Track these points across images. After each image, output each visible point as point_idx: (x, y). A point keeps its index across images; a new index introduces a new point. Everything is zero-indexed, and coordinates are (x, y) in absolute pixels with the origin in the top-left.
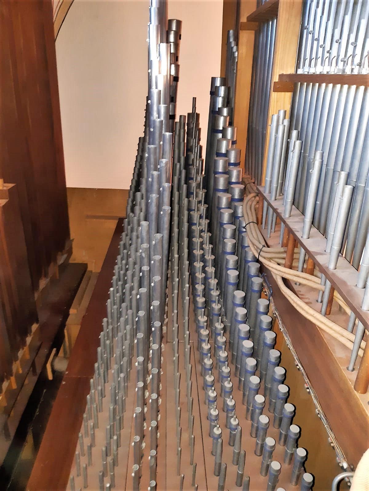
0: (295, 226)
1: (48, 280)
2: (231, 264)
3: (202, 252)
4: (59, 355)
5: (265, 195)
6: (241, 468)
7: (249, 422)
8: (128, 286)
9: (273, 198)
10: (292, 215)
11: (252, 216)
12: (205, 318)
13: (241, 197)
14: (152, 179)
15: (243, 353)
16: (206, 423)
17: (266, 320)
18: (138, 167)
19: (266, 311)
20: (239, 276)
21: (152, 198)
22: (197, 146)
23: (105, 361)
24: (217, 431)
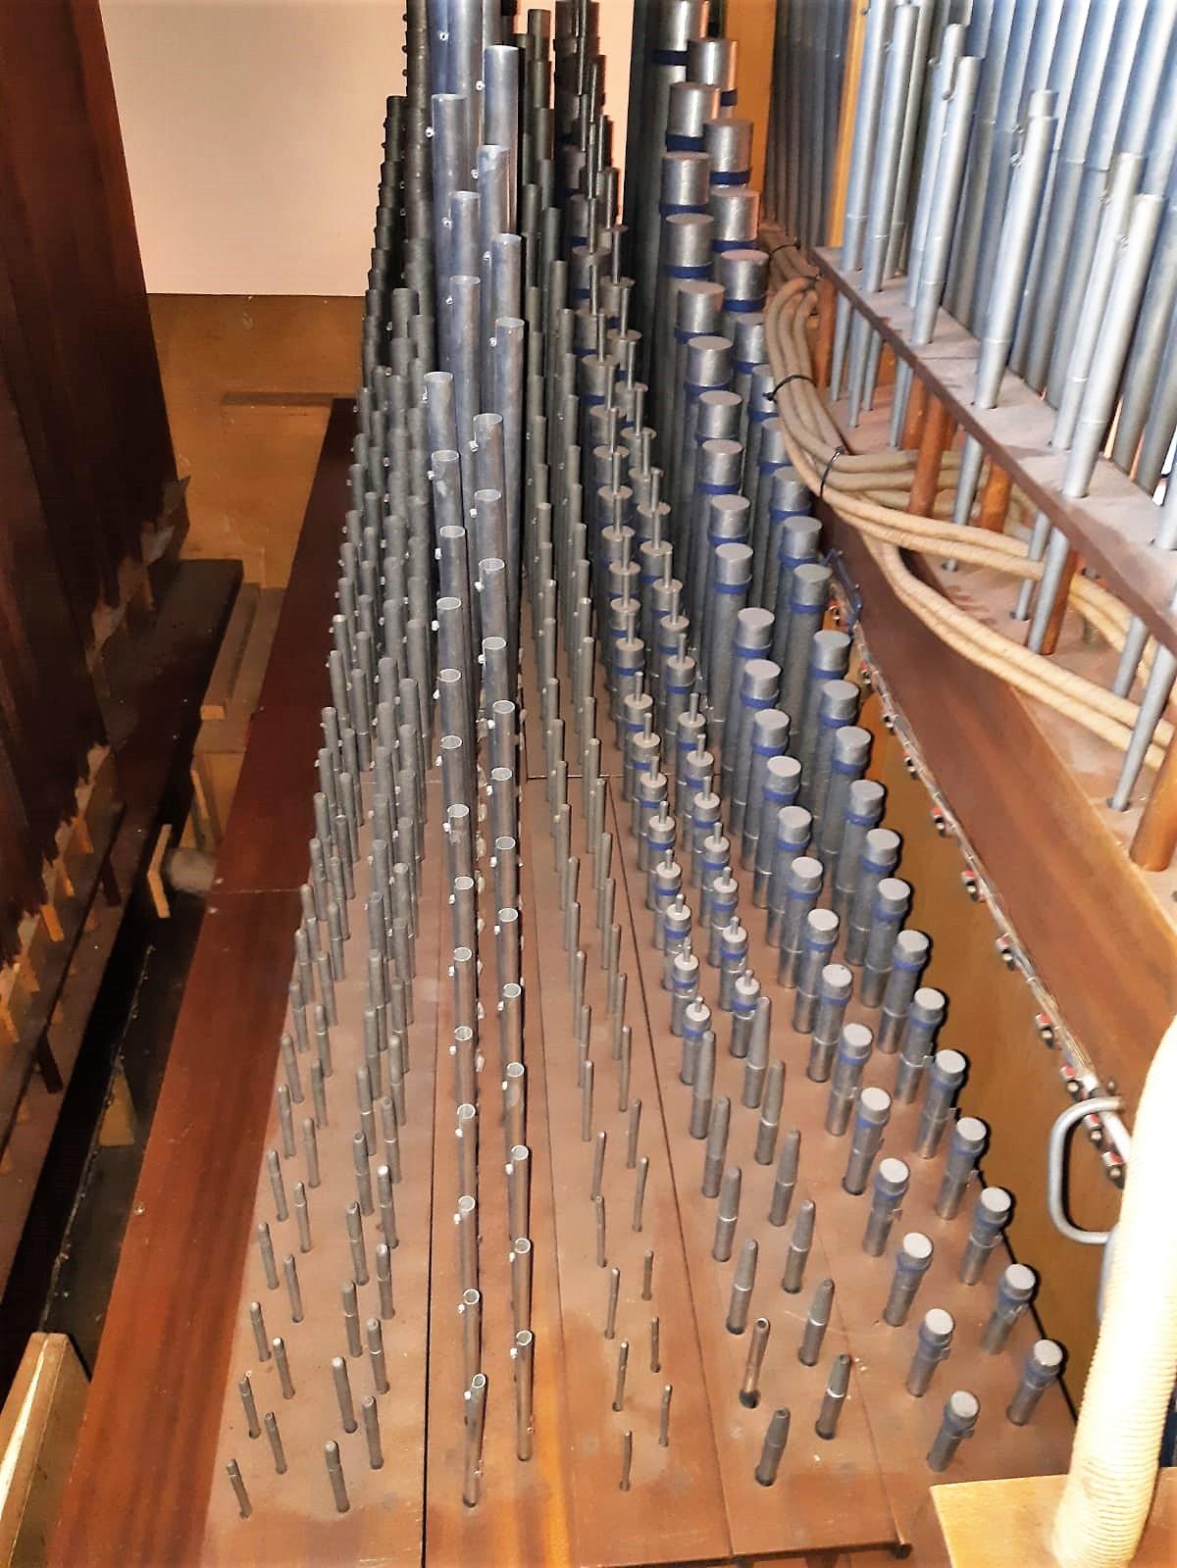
0: (950, 372)
1: (121, 611)
2: (727, 526)
3: (627, 492)
4: (183, 843)
5: (841, 274)
6: (770, 1113)
7: (787, 990)
8: (391, 605)
9: (871, 285)
10: (939, 338)
11: (798, 356)
12: (647, 701)
13: (757, 295)
14: (455, 218)
15: (767, 795)
16: (659, 1000)
17: (838, 694)
18: (390, 203)
19: (840, 668)
20: (751, 564)
21: (457, 287)
22: (596, 119)
23: (343, 837)
24: (696, 1015)
